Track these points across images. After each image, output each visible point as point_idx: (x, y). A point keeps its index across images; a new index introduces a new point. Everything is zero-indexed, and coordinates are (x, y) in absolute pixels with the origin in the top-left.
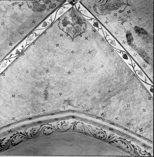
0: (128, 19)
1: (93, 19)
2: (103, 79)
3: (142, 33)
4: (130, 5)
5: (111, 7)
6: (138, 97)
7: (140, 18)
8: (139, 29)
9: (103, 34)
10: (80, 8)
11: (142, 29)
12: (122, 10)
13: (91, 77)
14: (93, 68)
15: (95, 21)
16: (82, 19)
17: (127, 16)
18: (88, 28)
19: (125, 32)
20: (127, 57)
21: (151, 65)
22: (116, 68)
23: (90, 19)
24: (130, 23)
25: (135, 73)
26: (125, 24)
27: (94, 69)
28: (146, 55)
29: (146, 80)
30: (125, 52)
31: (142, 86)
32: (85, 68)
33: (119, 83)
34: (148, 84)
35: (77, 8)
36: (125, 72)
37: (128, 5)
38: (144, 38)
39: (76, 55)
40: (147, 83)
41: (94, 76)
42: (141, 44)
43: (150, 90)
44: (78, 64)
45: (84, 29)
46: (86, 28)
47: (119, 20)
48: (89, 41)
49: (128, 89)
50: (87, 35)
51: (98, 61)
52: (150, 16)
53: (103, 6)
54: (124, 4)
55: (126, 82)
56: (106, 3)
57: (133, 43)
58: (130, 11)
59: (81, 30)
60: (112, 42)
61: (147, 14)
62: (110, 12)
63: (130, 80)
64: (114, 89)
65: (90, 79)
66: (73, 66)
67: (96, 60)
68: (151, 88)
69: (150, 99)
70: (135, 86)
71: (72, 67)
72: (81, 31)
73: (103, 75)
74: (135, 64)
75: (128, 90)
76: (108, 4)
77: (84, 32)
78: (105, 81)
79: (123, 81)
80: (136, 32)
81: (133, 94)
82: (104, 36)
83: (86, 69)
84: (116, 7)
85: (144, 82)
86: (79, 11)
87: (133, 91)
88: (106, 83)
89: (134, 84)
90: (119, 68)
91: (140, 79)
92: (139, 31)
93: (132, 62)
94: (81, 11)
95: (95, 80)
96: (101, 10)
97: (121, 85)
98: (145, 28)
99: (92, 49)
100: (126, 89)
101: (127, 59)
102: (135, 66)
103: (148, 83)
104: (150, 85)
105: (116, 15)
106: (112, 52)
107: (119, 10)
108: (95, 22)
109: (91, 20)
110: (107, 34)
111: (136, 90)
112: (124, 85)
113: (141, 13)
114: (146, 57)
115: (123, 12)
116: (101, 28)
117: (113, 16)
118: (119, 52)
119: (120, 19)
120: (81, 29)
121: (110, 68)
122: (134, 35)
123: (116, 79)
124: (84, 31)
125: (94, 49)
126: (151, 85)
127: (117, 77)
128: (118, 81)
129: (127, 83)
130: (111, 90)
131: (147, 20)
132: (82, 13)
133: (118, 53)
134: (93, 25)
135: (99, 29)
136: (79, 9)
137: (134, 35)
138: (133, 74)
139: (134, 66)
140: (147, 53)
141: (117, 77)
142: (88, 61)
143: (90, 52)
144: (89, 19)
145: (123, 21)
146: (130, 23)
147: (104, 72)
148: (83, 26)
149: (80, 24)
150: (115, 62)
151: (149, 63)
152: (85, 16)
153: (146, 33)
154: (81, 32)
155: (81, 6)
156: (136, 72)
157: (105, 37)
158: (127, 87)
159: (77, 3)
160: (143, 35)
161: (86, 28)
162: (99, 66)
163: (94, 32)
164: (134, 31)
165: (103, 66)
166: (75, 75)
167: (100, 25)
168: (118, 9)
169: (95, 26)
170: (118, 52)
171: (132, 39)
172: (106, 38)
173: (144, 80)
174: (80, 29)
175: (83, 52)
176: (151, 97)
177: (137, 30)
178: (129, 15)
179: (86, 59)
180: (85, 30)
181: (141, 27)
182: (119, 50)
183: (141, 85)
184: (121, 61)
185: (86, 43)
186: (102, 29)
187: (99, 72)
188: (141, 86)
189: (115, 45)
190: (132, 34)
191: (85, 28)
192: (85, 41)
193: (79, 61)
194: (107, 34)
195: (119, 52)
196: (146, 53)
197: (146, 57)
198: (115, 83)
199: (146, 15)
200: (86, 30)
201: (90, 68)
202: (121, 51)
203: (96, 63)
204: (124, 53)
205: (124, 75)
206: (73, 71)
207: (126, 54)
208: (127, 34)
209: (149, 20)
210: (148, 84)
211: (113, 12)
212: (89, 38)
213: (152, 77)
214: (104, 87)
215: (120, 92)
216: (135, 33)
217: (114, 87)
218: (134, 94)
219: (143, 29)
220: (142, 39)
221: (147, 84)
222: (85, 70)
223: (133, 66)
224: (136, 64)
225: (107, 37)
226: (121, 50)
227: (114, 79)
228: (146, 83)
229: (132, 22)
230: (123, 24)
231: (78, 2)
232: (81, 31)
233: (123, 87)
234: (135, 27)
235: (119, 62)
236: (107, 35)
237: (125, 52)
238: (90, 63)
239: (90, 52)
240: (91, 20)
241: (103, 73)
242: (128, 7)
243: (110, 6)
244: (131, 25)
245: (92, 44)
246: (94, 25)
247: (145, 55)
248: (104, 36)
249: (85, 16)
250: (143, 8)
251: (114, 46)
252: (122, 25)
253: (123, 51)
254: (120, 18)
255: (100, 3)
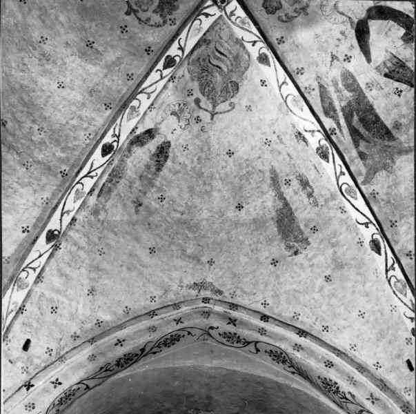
0: (183, 124)
1: (183, 52)
2: (29, 96)
3: (157, 161)
4: (212, 119)
5: (206, 79)
6: (17, 202)
7: (188, 147)
8: (165, 151)
9: (149, 84)
10: (207, 17)
11: (167, 157)
12: (202, 104)
13: (27, 63)
14: (50, 62)
15: (177, 59)
16: (174, 12)
17: (188, 118)
18: (152, 31)
19: (155, 125)
20: (106, 155)
21: (97, 203)
22: (67, 123)
23: (183, 46)
24: (175, 130)
25: (77, 183)
26: (173, 119)
27: (48, 67)
28: (114, 184)
29: (68, 212)
30: (118, 146)
31: (47, 201)
32: (47, 39)
33: (32, 140)
34: (61, 220)
35: (205, 11)
36: (63, 150)
37: (212, 116)
38: (148, 167)
39: (75, 8)
40: (63, 218)
41: (29, 70)
42: (135, 166)
43: (49, 231)
44: (53, 17)
45: (148, 19)
46: (152, 26)
47: (180, 105)
48: (120, 39)
49: (27, 169)
50: (132, 29)
51: (72, 70)
52: (195, 167)
53: (207, 61)
54: (214, 107)
55: (40, 157)
56: (214, 65)
57: (135, 149)
58: (201, 121)
59: (145, 11)
60: (133, 108)
61: (198, 160)
62: (196, 79)
63: (49, 169)
64: (14, 135)
65: (20, 60)
66: (44, 7)
67: (74, 65)
68: (55, 230)
69: (23, 232)
70: (39, 185)
71: (42, 5)
72: (141, 12)
73: (39, 93)
74: (96, 176)
75: (25, 169)
76: (212, 70)
77: (140, 19)
78: (25, 103)
79: (41, 150)
80: (158, 148)
81: (19, 187)
82: (146, 88)
83: (45, 43)
84: (206, 90)
85: (63, 209)
86: (198, 15)
87: (27, 186)
88: (20, 108)
89: (44, 180)
90: (68, 131)
91: (66, 199)
92: (161, 152)
93: (99, 167)
94: (199, 21)
95: (21, 74)
96: (199, 58)
97: (28, 147)
98: (169, 163)
99: (100, 49)
100: (24, 165)
101: (103, 155)
102: (92, 177)
103: (63, 220)
104: (61, 226)
105: (190, 93)
106: (105, 105)
107: (200, 96)
108: (261, 53)
109: (181, 49)
110: (152, 92)
111: (31, 192)
112: (31, 157)
113: (198, 146)
114: (109, 185)
115: (196, 108)
116: (164, 75)
117: (187, 89)
118: (114, 132)
119: (182, 105)
120: (147, 10)
121: (63, 108)
122: (152, 146)
123: (39, 130)
124: (143, 21)
125: (101, 54)
126: (61, 229)
127: (46, 129)
128: (36, 138)
129: (39, 162)
130: (7, 126)
131: (186, 163)
132: (194, 24)
133: (120, 146)
134: (166, 55)
135: (161, 71)
136: (203, 14)
137: (152, 146)
138: (65, 170)
139: (91, 174)
140: (118, 184)
141: (46, 129)
142: (67, 43)
143: (90, 45)
144: (182, 44)
145: (178, 113)
146: (175, 130)
147: (49, 94)
148: (157, 18)
149: (159, 6)
150: (80, 118)
151: (100, 198)
152: (189, 31)
153: (159, 170)
154: (138, 11)
155: (211, 20)
156: (79, 185)
157: (144, 89)
158: (29, 164)
159: (218, 11)
160: (153, 163)
161: (152, 26)
162: (60, 77)
163: (146, 50)
164: (160, 143)
165: (63, 87)
166: (20, 17)
167: (170, 73)
168: (204, 95)
169: (166, 59)
170: (114, 129)
171: (142, 144)
172: (141, 92)
173: (66, 209)
174: (146, 8)
175: (87, 25)
176: (28, 231)
177: (162, 148)
178: (193, 121)
179: (72, 37)
180: (146, 23)
181: (171, 155)
182: (120, 130)
183: (47, 199)
184: (90, 134)
185: (111, 29)
186: (162, 78)
187: (43, 80)
188: (45, 199)
189: (129, 119)
190: (153, 141)
191: (151, 23)
192: (115, 27)
193: (62, 18)
194: (152, 92)
195: (114, 132)
196: (118, 182)
197: (109, 185)
198: (28, 130)
199: (195, 159)
200: (146, 26)
201: (49, 55)
202: (118, 137)
203: (66, 69)
204: (115, 144)
205: (57, 149)
206: (30, 10)
207: (115, 149)
208: (152, 129)
209: (187, 166)
210: (61, 220)
211: (195, 86)
212: (126, 37)
213: (375, 103)
214: (10, 105)
215: (12, 154)
216: (156, 148)
217: (18, 132)
218: (21, 190)
219: (166, 161)
220: (146, 163)
221: (59, 218)
222: (40, 42)
223: (89, 173)
224: (96, 179)
225: (146, 96)
226: (119, 135)
227: (39, 125)
228: (62, 215)
229: (179, 131)
230: (173, 116)
231: (221, 12)
232: (141, 12)
233: (25, 156)
234: (169, 142)
235: (86, 129)
236: (148, 94)
237: (118, 146)
238: (62, 50)
239: (90, 45)
240: (179, 49)
241: (43, 91)
242: (209, 115)
243: (207, 75)
244: (172, 133)
245: (112, 46)
246: (168, 56)
247: (114, 181)
248: (146, 88)
249: (189, 31)
250: (209, 149)
251: (125, 116)
252: (169, 113)
253: (118, 142)
254: (184, 104)
255: (213, 52)
